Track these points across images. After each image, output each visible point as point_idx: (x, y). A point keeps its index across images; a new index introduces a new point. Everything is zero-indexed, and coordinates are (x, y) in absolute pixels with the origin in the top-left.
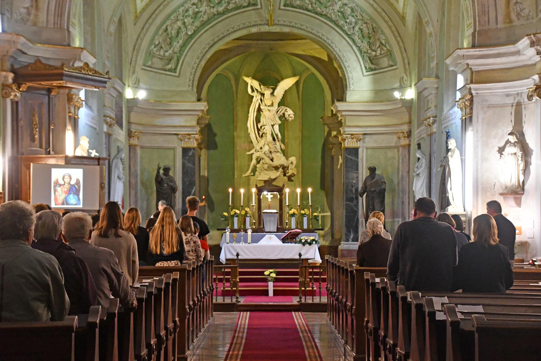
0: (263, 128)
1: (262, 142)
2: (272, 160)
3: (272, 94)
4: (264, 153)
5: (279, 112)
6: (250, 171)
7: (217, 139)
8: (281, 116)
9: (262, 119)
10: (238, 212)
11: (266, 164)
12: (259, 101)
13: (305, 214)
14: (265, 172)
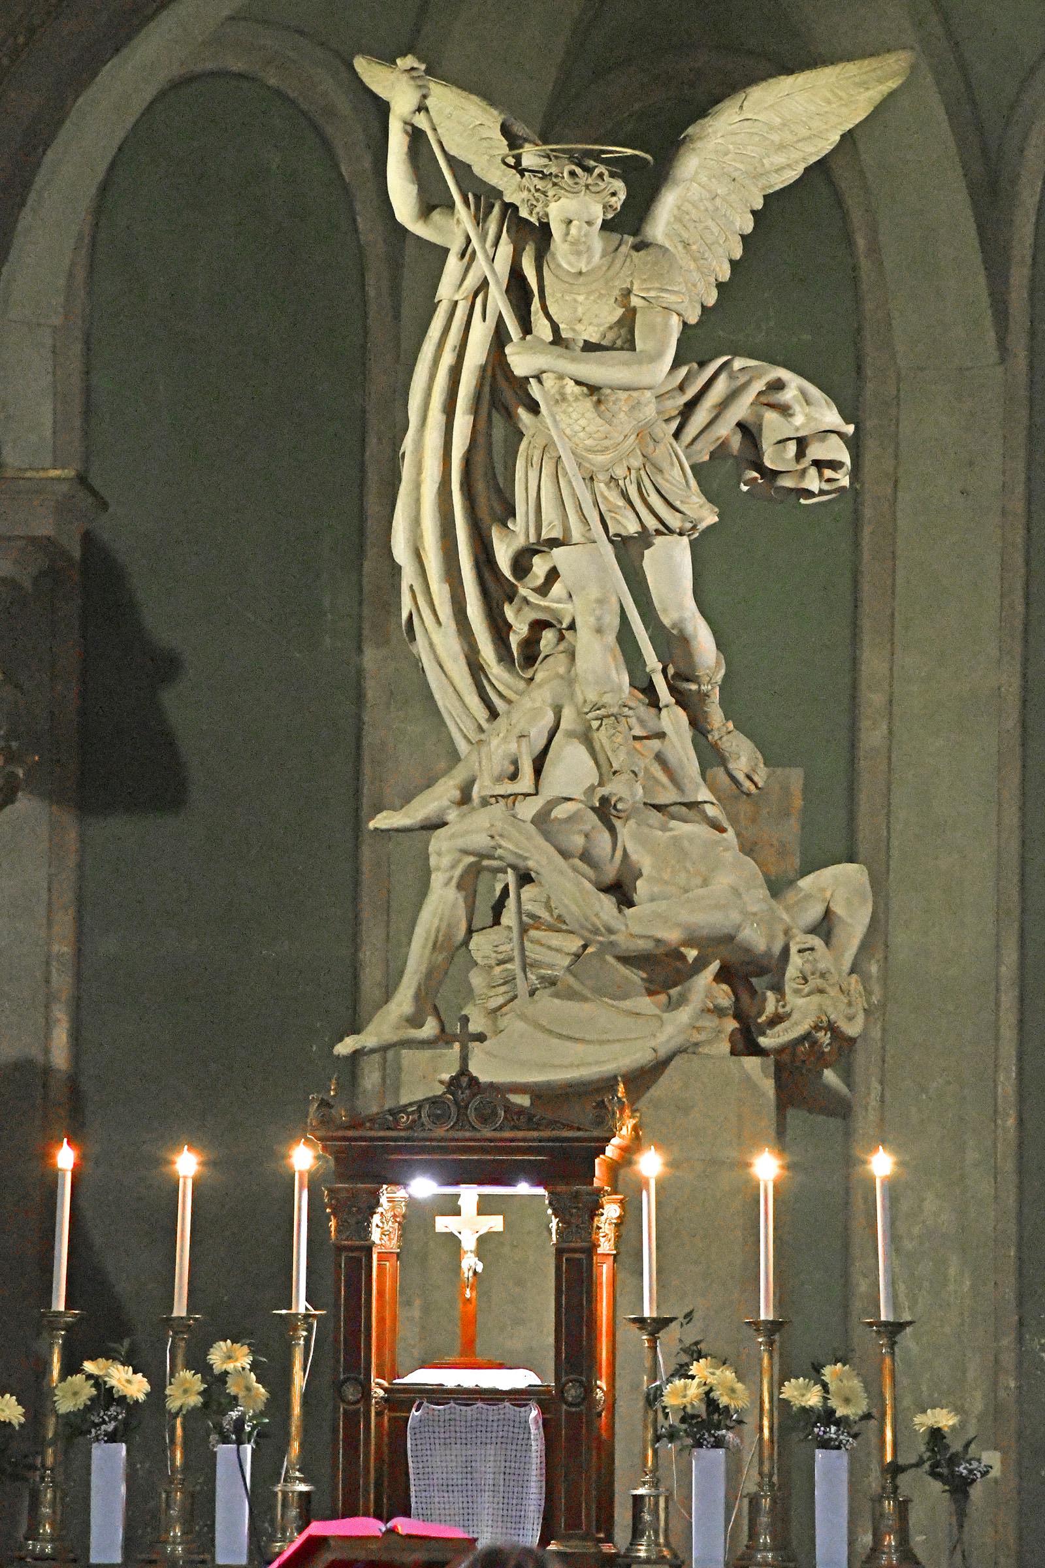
0: (540, 567)
1: (531, 707)
2: (620, 891)
3: (628, 223)
4: (542, 820)
5: (700, 417)
6: (403, 1002)
7: (180, 706)
8: (720, 451)
9: (528, 482)
10: (131, 1384)
11: (559, 925)
12: (498, 301)
13: (828, 1416)
14: (548, 1005)
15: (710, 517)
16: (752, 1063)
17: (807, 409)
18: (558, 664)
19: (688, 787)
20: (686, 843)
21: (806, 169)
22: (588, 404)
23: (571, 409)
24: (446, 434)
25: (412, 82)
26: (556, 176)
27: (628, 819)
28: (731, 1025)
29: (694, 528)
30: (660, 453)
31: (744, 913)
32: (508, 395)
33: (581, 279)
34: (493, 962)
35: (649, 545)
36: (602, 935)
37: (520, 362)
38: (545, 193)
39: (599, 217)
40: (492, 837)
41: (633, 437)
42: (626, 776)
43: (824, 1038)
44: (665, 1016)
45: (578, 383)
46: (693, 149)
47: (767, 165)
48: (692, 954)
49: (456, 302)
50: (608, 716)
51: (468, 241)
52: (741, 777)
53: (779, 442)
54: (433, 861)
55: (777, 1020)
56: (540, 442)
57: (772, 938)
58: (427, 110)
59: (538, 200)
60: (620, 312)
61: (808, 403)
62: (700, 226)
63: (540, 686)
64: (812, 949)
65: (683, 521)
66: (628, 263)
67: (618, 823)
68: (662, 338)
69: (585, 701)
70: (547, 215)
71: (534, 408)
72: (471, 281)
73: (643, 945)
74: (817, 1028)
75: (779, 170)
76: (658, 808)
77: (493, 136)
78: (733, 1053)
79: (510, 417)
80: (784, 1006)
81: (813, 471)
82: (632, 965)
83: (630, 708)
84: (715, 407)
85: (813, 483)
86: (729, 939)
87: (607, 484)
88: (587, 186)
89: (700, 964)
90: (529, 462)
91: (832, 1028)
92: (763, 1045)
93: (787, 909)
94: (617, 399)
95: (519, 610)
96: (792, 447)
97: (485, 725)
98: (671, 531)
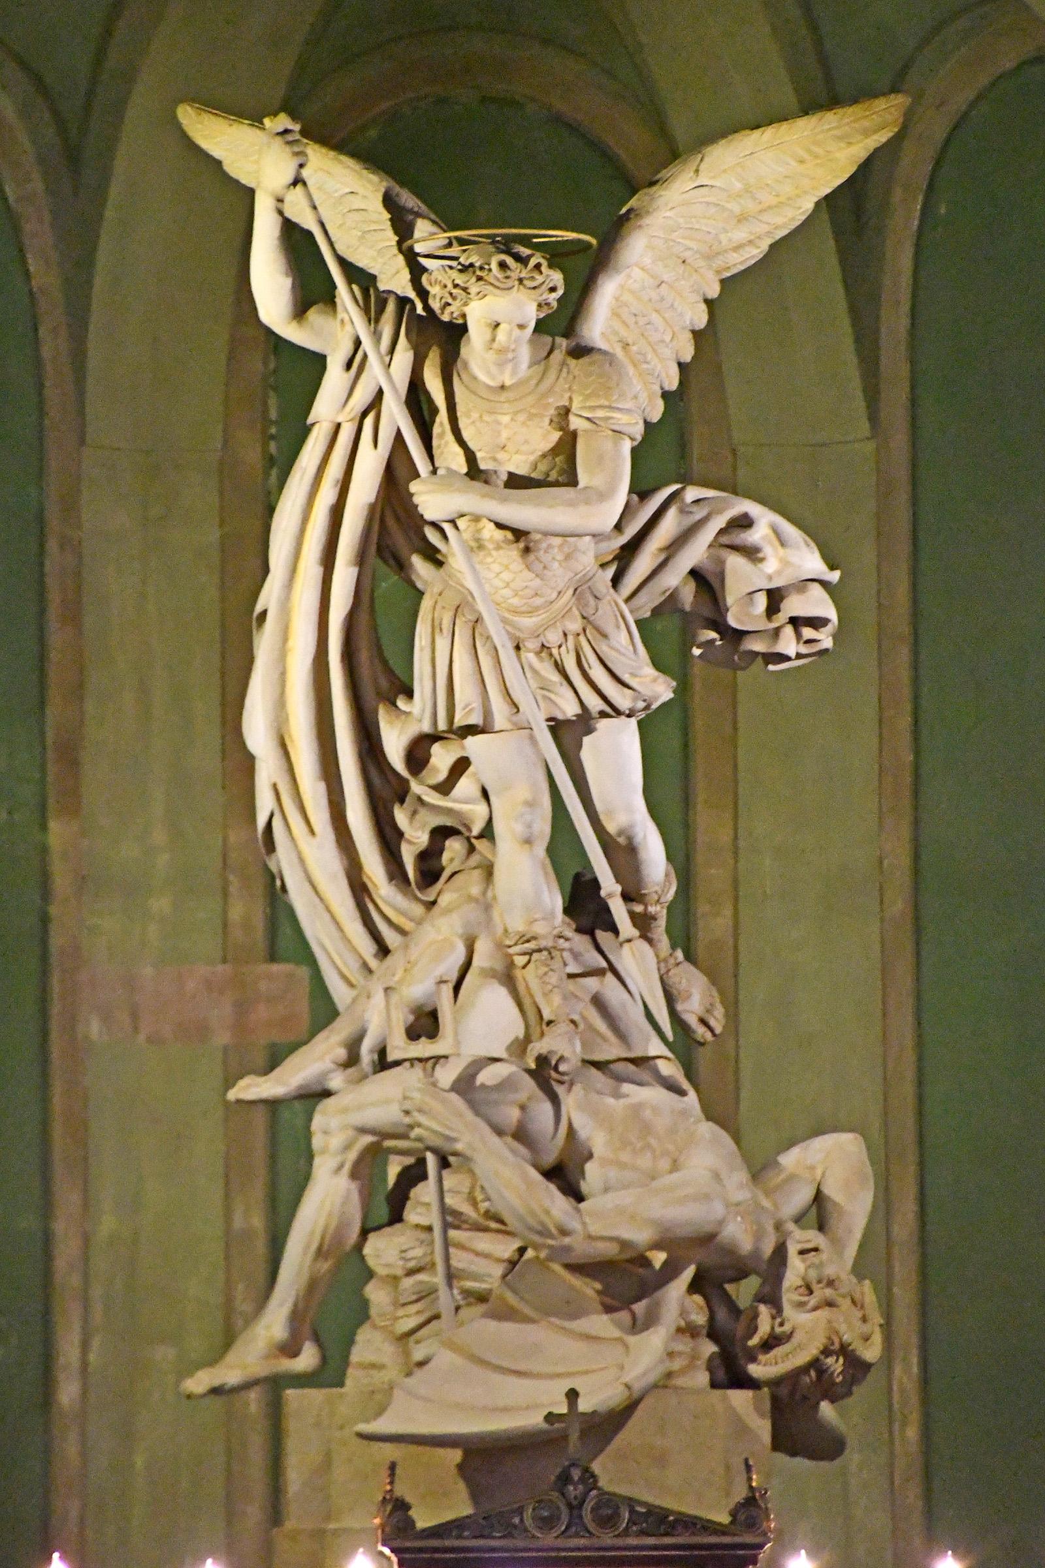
0: (441, 758)
2: (564, 1175)
3: (561, 326)
4: (465, 1085)
6: (273, 1323)
9: (434, 654)
14: (482, 1330)
15: (662, 690)
16: (740, 1398)
17: (781, 551)
18: (472, 883)
19: (635, 1037)
20: (648, 1114)
21: (771, 246)
22: (513, 553)
23: (489, 560)
24: (329, 590)
25: (288, 149)
26: (481, 268)
27: (572, 1084)
28: (709, 1348)
29: (647, 707)
30: (605, 615)
31: (727, 1205)
32: (399, 540)
33: (504, 396)
34: (399, 1272)
35: (590, 731)
36: (552, 1236)
37: (430, 500)
38: (465, 289)
39: (531, 314)
40: (407, 1113)
41: (571, 591)
42: (563, 1027)
43: (835, 1365)
44: (632, 1340)
45: (500, 526)
46: (640, 226)
47: (724, 242)
48: (659, 1258)
49: (339, 426)
50: (539, 950)
51: (358, 343)
52: (692, 1021)
53: (750, 594)
54: (317, 1142)
55: (770, 1343)
56: (451, 599)
57: (758, 1236)
58: (305, 184)
59: (454, 298)
60: (556, 436)
61: (783, 544)
62: (642, 321)
63: (448, 911)
64: (816, 1250)
65: (635, 699)
66: (564, 374)
67: (560, 1090)
68: (609, 472)
69: (506, 931)
70: (464, 316)
71: (434, 557)
72: (363, 395)
73: (609, 1250)
74: (826, 1352)
75: (738, 248)
76: (597, 1065)
77: (370, 208)
78: (714, 1385)
79: (402, 567)
80: (781, 1324)
81: (789, 630)
82: (588, 1275)
83: (567, 939)
84: (661, 550)
85: (788, 645)
86: (707, 1239)
87: (538, 654)
88: (521, 280)
89: (670, 1271)
90: (435, 628)
91: (844, 1350)
92: (755, 1375)
93: (767, 1193)
94: (550, 546)
95: (414, 813)
96: (762, 602)
97: (373, 963)
98: (618, 713)
